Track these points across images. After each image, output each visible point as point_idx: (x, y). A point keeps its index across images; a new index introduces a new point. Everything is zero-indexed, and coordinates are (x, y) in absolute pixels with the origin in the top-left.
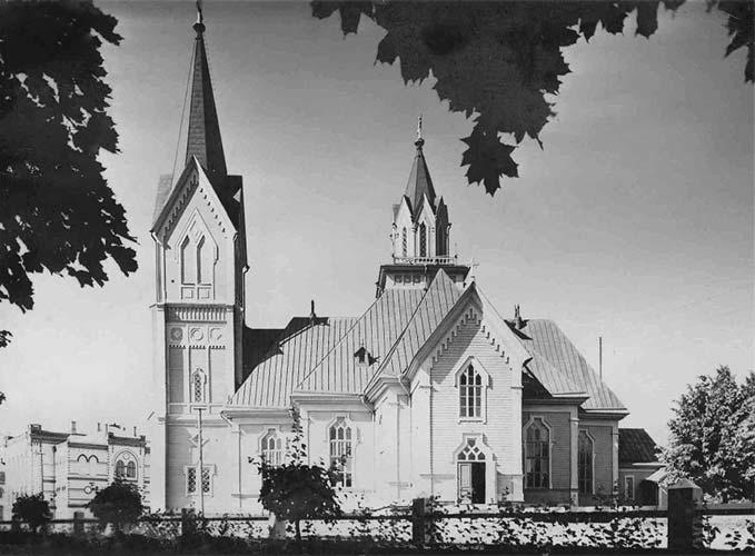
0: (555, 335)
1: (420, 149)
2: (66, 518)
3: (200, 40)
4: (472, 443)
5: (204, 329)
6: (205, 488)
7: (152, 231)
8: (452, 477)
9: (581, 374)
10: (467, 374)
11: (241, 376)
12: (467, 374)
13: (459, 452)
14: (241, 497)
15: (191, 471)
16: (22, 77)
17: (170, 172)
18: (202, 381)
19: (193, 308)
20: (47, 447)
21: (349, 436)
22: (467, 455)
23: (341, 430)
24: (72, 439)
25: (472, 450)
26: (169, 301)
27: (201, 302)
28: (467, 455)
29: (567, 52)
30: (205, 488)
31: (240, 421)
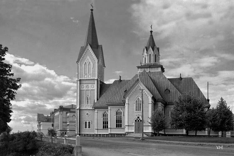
0: (192, 82)
1: (151, 33)
2: (100, 130)
3: (92, 13)
4: (138, 117)
5: (90, 85)
6: (89, 127)
7: (77, 62)
8: (145, 126)
9: (197, 93)
10: (137, 100)
11: (99, 96)
12: (137, 100)
13: (135, 120)
14: (97, 129)
15: (86, 123)
16: (8, 88)
17: (83, 46)
18: (89, 99)
19: (87, 80)
20: (65, 112)
21: (121, 114)
22: (137, 120)
23: (106, 115)
24: (71, 110)
25: (138, 119)
26: (81, 79)
27: (89, 78)
28: (137, 120)
29: (10, 118)
30: (89, 127)
31: (98, 110)
